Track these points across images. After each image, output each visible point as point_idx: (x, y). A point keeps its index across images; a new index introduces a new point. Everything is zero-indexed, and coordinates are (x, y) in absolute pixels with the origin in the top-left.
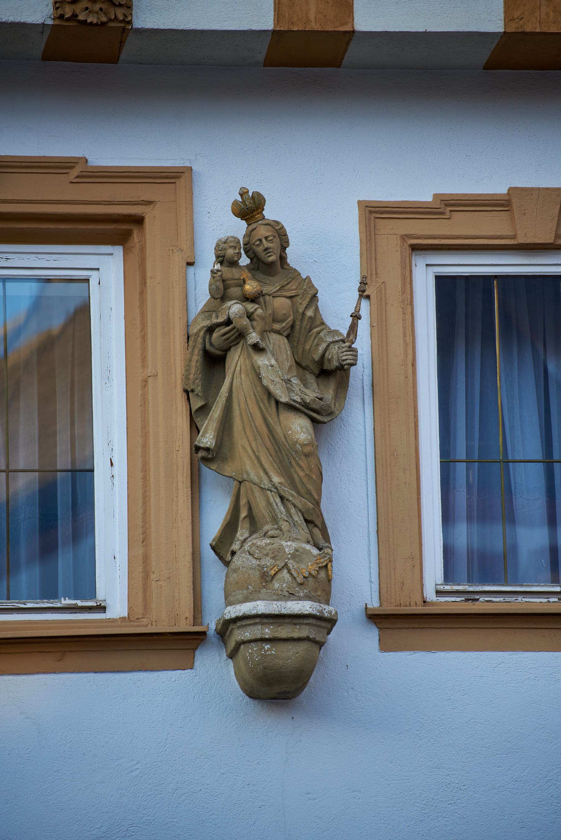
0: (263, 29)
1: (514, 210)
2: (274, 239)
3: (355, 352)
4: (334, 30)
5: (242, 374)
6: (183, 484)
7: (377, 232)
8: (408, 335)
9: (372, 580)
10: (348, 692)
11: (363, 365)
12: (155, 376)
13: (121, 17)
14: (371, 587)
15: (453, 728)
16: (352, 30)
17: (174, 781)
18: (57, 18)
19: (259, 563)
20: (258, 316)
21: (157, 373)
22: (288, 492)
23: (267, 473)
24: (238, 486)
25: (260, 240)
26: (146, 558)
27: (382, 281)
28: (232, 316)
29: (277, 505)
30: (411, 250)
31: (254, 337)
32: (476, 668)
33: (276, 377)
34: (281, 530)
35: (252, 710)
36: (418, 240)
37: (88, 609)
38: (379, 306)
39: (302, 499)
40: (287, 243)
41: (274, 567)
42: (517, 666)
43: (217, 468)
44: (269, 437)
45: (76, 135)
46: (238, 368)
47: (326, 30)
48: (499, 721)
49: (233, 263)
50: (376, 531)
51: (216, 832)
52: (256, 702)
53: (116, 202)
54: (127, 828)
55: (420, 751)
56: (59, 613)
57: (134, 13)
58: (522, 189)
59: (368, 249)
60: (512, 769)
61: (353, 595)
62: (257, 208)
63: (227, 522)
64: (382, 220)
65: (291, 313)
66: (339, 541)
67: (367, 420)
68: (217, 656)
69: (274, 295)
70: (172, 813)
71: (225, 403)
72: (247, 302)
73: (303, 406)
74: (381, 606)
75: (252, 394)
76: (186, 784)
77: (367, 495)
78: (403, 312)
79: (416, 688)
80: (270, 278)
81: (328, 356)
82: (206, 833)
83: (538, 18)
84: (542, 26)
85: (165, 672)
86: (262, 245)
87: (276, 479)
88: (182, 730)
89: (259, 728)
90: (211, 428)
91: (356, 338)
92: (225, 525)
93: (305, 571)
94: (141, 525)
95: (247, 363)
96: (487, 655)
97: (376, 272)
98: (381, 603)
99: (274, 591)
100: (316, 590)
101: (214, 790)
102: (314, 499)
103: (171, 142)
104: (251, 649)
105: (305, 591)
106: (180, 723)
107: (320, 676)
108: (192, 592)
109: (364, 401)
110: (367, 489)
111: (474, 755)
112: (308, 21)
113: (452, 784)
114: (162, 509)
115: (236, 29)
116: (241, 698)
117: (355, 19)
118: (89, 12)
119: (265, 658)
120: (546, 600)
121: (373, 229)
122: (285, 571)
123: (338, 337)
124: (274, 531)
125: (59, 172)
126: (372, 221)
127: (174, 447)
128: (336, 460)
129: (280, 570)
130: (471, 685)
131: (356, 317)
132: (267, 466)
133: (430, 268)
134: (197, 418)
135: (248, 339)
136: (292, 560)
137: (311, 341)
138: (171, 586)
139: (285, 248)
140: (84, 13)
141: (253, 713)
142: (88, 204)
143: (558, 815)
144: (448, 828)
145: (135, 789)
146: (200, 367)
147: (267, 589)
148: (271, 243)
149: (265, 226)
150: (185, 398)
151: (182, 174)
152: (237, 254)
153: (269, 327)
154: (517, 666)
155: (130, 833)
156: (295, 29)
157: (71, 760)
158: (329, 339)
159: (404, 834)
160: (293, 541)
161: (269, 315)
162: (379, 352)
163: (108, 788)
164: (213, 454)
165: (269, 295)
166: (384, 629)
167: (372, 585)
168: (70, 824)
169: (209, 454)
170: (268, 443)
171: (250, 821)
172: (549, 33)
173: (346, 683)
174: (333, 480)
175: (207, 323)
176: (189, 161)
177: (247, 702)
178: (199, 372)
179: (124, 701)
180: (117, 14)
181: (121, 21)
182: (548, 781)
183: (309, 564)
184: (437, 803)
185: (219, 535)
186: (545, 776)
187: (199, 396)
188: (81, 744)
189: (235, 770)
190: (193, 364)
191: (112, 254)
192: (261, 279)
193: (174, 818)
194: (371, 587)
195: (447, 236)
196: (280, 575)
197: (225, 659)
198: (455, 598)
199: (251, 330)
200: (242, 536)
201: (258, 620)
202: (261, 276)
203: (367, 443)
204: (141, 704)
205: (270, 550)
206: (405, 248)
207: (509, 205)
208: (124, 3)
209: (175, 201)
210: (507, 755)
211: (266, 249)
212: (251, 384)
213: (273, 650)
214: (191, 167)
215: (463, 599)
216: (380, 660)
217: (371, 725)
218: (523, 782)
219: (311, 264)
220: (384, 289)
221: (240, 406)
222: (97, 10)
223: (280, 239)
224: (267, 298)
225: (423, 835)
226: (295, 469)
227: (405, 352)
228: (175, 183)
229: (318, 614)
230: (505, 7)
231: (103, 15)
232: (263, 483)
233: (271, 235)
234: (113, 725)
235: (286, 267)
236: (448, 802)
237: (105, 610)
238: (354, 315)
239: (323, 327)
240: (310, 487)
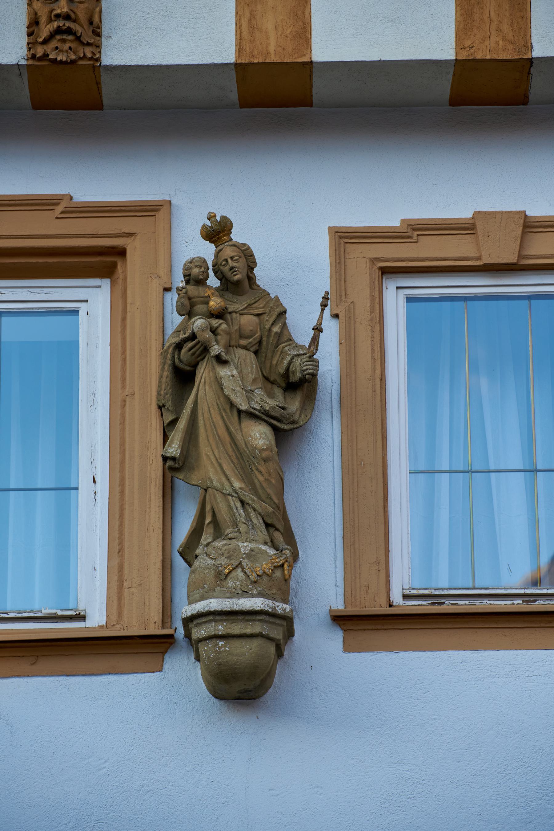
0: (225, 62)
1: (479, 233)
2: (240, 259)
3: (316, 362)
4: (292, 61)
5: (206, 386)
6: (156, 496)
7: (347, 256)
8: (376, 352)
9: (337, 584)
10: (312, 692)
11: (332, 380)
12: (132, 395)
13: (89, 55)
14: (337, 590)
15: (414, 724)
16: (310, 61)
17: (140, 778)
18: (30, 58)
19: (214, 562)
20: (222, 330)
21: (134, 392)
22: (248, 497)
23: (228, 479)
24: (204, 494)
25: (226, 260)
26: (121, 568)
27: (351, 301)
28: (196, 330)
29: (237, 509)
30: (380, 273)
31: (216, 349)
32: (438, 667)
33: (237, 386)
34: (240, 533)
35: (218, 710)
36: (387, 263)
37: (69, 619)
38: (347, 324)
39: (262, 503)
40: (254, 264)
41: (228, 566)
42: (477, 665)
43: (184, 477)
44: (231, 445)
45: (63, 175)
46: (203, 380)
47: (285, 61)
48: (459, 717)
49: (200, 282)
50: (342, 537)
51: (180, 827)
52: (222, 702)
54: (93, 824)
55: (381, 748)
56: (41, 622)
57: (102, 51)
58: (486, 213)
59: (337, 271)
60: (471, 764)
61: (319, 599)
62: (222, 230)
63: (193, 528)
64: (352, 245)
66: (307, 548)
67: (335, 432)
68: (186, 659)
69: (241, 312)
70: (137, 809)
71: (190, 414)
72: (213, 318)
73: (263, 413)
74: (345, 608)
75: (215, 404)
76: (152, 781)
77: (334, 503)
78: (371, 329)
79: (378, 687)
80: (239, 297)
81: (292, 368)
82: (171, 828)
83: (489, 46)
84: (492, 54)
85: (135, 675)
86: (228, 265)
87: (237, 485)
89: (225, 727)
90: (177, 439)
91: (317, 350)
92: (190, 532)
93: (258, 569)
94: (117, 536)
95: (211, 375)
96: (449, 654)
97: (345, 293)
98: (345, 605)
99: (228, 589)
100: (270, 588)
101: (179, 787)
102: (275, 503)
103: (152, 179)
104: (207, 646)
105: (259, 589)
106: (148, 724)
107: (285, 677)
108: (161, 597)
109: (332, 414)
110: (334, 497)
111: (434, 751)
112: (268, 54)
113: (412, 779)
114: (136, 519)
115: (200, 63)
116: (207, 699)
117: (313, 51)
118: (59, 51)
119: (219, 654)
120: (511, 602)
121: (342, 253)
122: (239, 570)
123: (303, 351)
124: (234, 534)
125: (45, 209)
126: (342, 245)
127: (149, 461)
128: (305, 471)
129: (234, 569)
130: (432, 683)
131: (318, 330)
132: (228, 472)
134: (169, 432)
135: (211, 351)
136: (247, 559)
137: (278, 356)
138: (142, 592)
139: (252, 269)
140: (54, 52)
141: (218, 713)
142: (73, 238)
143: (516, 808)
144: (407, 821)
145: (102, 786)
147: (221, 587)
148: (236, 262)
149: (231, 247)
150: (159, 414)
151: (161, 207)
154: (477, 665)
155: (97, 829)
156: (256, 61)
157: (41, 759)
158: (293, 353)
159: (363, 827)
160: (250, 542)
162: (346, 367)
163: (76, 785)
164: (179, 463)
165: (236, 313)
166: (348, 631)
167: (338, 589)
168: (39, 820)
170: (230, 450)
171: (214, 817)
172: (499, 59)
173: (310, 683)
174: (302, 489)
175: (177, 340)
176: (169, 196)
177: (213, 703)
178: (169, 387)
179: (95, 702)
180: (86, 52)
181: (91, 59)
182: (507, 775)
183: (264, 563)
184: (396, 797)
185: (185, 541)
186: (503, 770)
187: (170, 410)
188: (52, 744)
189: (200, 768)
190: (164, 380)
191: (100, 287)
192: (229, 299)
193: (139, 815)
194: (337, 590)
195: (415, 259)
196: (234, 574)
197: (193, 662)
198: (422, 602)
199: (214, 343)
200: (205, 540)
201: (211, 617)
202: (230, 295)
203: (335, 454)
205: (225, 550)
206: (374, 271)
207: (474, 228)
208: (92, 42)
209: (155, 232)
210: (466, 751)
211: (232, 268)
212: (214, 394)
213: (227, 647)
214: (170, 201)
215: (430, 602)
216: (344, 661)
217: (334, 724)
218: (482, 776)
219: (284, 287)
220: (353, 309)
221: (203, 416)
222: (66, 49)
223: (246, 260)
224: (234, 315)
225: (382, 828)
226: (255, 474)
227: (373, 368)
228: (155, 216)
229: (270, 610)
230: (456, 37)
231: (72, 53)
232: (225, 488)
233: (236, 255)
234: (83, 726)
235: (255, 287)
236: (408, 797)
237: (85, 619)
238: (315, 328)
239: (290, 342)
240: (269, 491)
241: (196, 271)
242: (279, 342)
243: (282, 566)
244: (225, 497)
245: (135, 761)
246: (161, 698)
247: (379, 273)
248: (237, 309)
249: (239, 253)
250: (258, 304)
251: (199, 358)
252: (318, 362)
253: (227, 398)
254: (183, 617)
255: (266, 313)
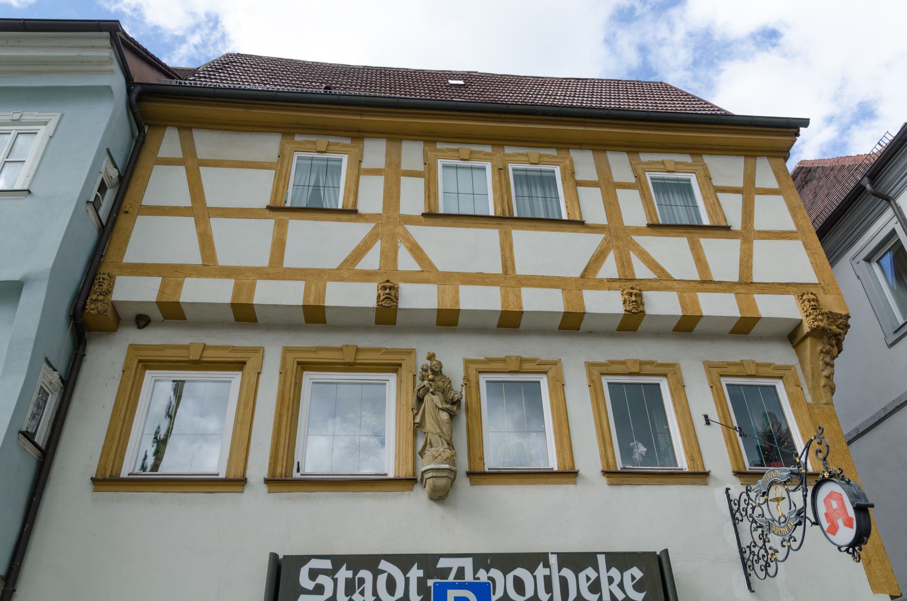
13: (395, 305)
31: (431, 390)
112: (447, 306)
243: (453, 456)
253: (435, 404)
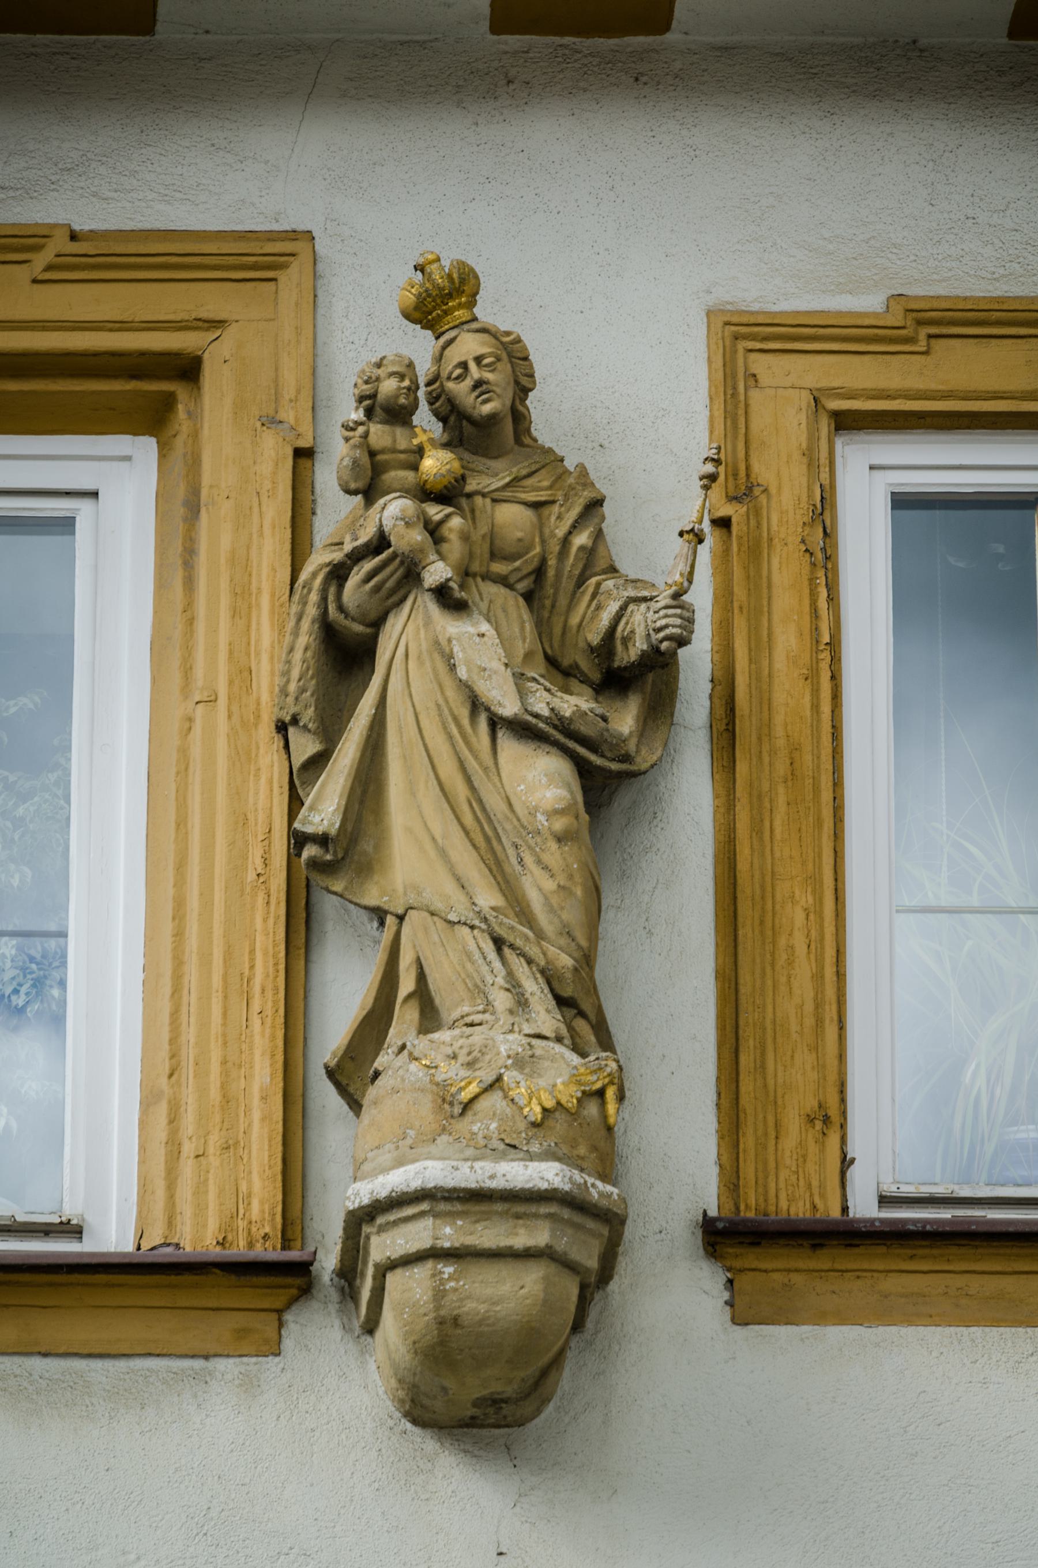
12: (210, 701)
25: (464, 365)
28: (388, 525)
30: (833, 426)
31: (437, 572)
37: (43, 1235)
43: (346, 888)
52: (428, 1433)
53: (137, 324)
65: (537, 540)
69: (496, 495)
73: (555, 727)
75: (432, 705)
88: (246, 1491)
92: (361, 1018)
100: (574, 1145)
133: (877, 474)
134: (305, 786)
146: (312, 663)
148: (489, 371)
151: (292, 259)
152: (405, 391)
153: (481, 566)
161: (481, 538)
169: (327, 851)
178: (310, 672)
190: (298, 655)
191: (128, 458)
199: (433, 557)
201: (425, 1206)
204: (151, 1431)
205: (461, 1047)
223: (512, 367)
224: (479, 500)
233: (489, 353)
234: (83, 1473)
235: (527, 440)
241: (389, 387)
242: (588, 573)
243: (601, 1093)
244: (453, 930)
245: (210, 1560)
246: (275, 1419)
247: (829, 425)
248: (485, 487)
249: (498, 349)
250: (537, 480)
251: (390, 601)
252: (693, 612)
254: (351, 1208)
255: (558, 500)
